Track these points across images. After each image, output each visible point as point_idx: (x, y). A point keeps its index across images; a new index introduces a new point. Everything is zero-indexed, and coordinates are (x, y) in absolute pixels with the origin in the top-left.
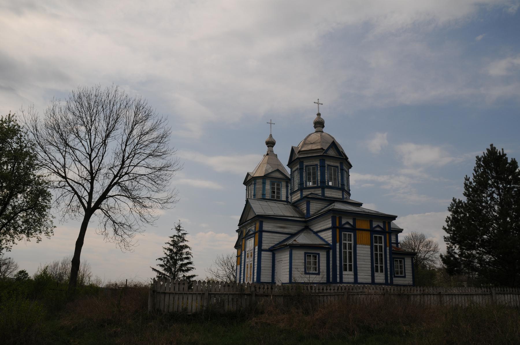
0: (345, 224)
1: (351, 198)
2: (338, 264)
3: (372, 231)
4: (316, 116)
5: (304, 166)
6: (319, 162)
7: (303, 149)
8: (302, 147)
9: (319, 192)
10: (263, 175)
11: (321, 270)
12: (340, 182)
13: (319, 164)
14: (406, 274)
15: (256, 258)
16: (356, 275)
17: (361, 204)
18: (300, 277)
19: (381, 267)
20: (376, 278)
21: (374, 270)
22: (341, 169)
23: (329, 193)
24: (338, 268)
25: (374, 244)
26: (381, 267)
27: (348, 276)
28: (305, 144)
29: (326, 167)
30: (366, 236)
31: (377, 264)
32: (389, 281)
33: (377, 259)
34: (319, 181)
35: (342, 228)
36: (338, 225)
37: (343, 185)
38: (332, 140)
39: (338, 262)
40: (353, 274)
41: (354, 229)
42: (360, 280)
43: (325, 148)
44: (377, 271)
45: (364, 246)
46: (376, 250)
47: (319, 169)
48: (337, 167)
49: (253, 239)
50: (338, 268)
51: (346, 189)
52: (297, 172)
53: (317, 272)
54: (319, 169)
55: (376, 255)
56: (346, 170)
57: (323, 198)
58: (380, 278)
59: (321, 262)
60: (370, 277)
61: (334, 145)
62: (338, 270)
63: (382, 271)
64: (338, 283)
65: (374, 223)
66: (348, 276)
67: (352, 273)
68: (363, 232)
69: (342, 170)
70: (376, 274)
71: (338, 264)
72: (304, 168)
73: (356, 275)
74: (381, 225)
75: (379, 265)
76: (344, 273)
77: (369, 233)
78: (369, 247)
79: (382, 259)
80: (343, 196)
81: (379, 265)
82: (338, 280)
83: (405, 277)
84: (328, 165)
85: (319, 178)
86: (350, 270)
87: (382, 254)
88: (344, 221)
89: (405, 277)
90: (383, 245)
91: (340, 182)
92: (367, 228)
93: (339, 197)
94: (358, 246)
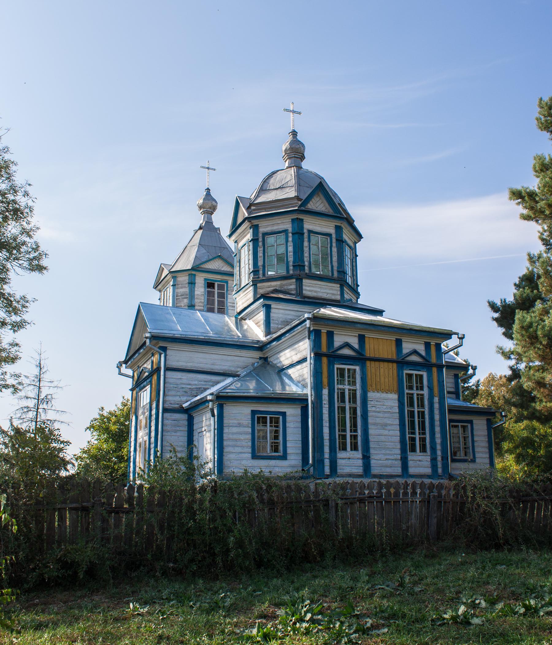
0: (341, 347)
1: (360, 301)
2: (326, 436)
3: (402, 363)
4: (290, 138)
5: (260, 235)
6: (291, 225)
7: (259, 200)
8: (257, 196)
9: (291, 285)
10: (189, 267)
11: (289, 451)
12: (335, 268)
13: (290, 230)
14: (477, 455)
15: (153, 428)
16: (366, 458)
17: (379, 312)
18: (241, 462)
19: (423, 440)
20: (410, 463)
21: (407, 446)
22: (337, 240)
23: (312, 288)
24: (327, 443)
25: (406, 391)
26: (423, 440)
27: (349, 462)
28: (263, 189)
29: (306, 235)
30: (386, 373)
31: (414, 433)
32: (440, 471)
33: (412, 423)
34: (291, 264)
35: (334, 356)
36: (324, 349)
37: (342, 272)
38: (319, 181)
39: (326, 430)
40: (360, 456)
41: (360, 358)
42: (375, 470)
43: (304, 197)
44: (413, 450)
45: (384, 395)
46: (411, 404)
47: (290, 239)
48: (329, 235)
49: (148, 388)
50: (327, 443)
51: (349, 280)
52: (246, 248)
53: (281, 454)
54: (290, 239)
55: (412, 414)
56: (351, 244)
57: (298, 299)
58: (420, 463)
59: (289, 431)
60: (399, 463)
61: (321, 188)
62: (327, 450)
63: (423, 449)
64: (327, 477)
65: (404, 345)
66: (349, 462)
67: (358, 454)
68: (382, 364)
69: (340, 241)
70: (411, 457)
71: (326, 436)
72: (260, 239)
73: (366, 458)
74: (421, 349)
75: (417, 436)
76: (341, 455)
77: (395, 365)
78: (395, 396)
79: (423, 423)
80: (342, 294)
81: (417, 436)
82: (327, 470)
83: (473, 461)
84: (310, 232)
85: (492, 434)
86: (355, 447)
87: (423, 413)
88: (338, 341)
89: (473, 461)
90: (426, 392)
91: (335, 268)
92: (390, 357)
93: (333, 297)
94: (370, 395)
